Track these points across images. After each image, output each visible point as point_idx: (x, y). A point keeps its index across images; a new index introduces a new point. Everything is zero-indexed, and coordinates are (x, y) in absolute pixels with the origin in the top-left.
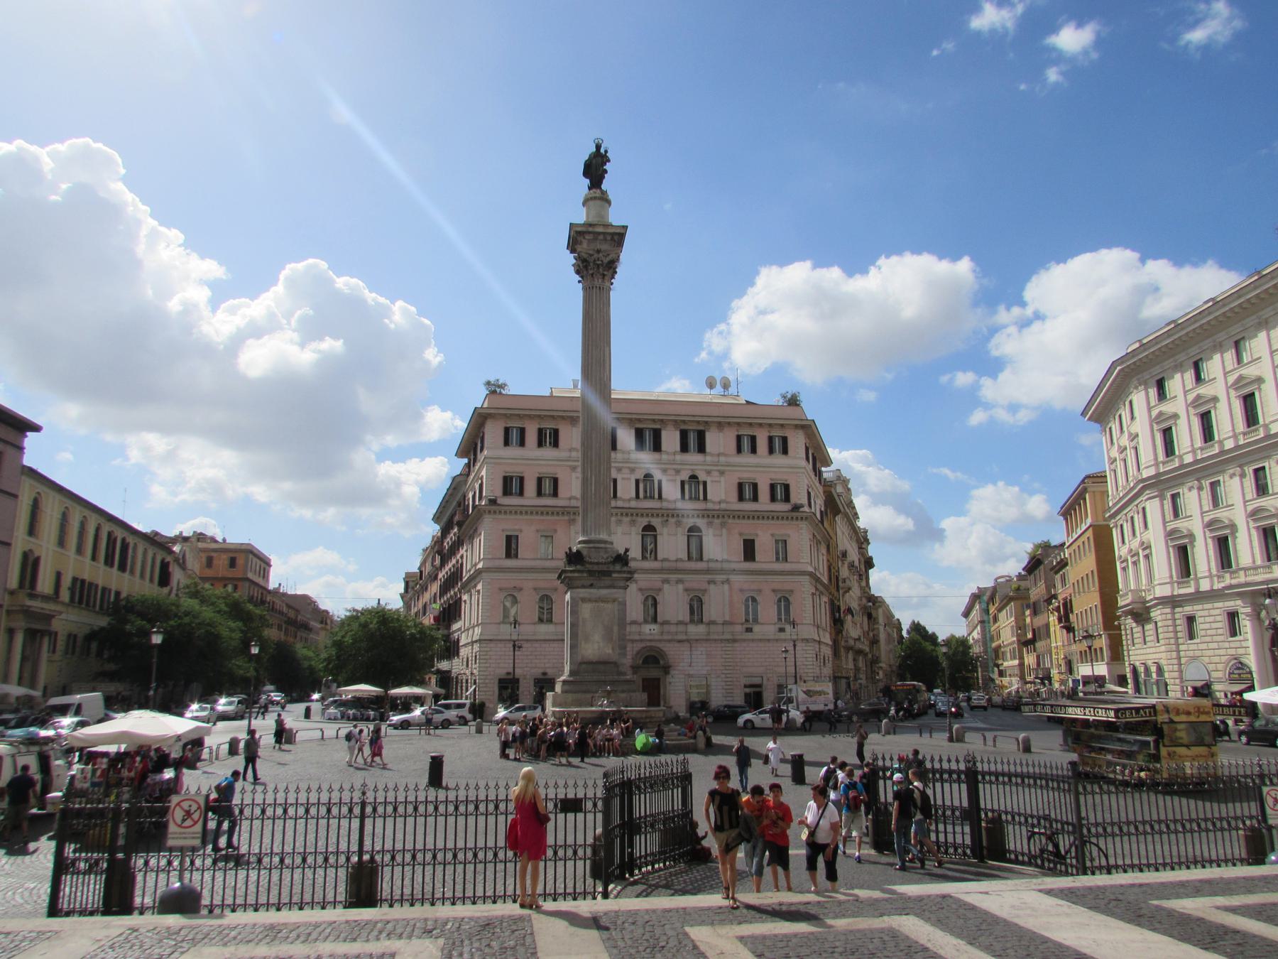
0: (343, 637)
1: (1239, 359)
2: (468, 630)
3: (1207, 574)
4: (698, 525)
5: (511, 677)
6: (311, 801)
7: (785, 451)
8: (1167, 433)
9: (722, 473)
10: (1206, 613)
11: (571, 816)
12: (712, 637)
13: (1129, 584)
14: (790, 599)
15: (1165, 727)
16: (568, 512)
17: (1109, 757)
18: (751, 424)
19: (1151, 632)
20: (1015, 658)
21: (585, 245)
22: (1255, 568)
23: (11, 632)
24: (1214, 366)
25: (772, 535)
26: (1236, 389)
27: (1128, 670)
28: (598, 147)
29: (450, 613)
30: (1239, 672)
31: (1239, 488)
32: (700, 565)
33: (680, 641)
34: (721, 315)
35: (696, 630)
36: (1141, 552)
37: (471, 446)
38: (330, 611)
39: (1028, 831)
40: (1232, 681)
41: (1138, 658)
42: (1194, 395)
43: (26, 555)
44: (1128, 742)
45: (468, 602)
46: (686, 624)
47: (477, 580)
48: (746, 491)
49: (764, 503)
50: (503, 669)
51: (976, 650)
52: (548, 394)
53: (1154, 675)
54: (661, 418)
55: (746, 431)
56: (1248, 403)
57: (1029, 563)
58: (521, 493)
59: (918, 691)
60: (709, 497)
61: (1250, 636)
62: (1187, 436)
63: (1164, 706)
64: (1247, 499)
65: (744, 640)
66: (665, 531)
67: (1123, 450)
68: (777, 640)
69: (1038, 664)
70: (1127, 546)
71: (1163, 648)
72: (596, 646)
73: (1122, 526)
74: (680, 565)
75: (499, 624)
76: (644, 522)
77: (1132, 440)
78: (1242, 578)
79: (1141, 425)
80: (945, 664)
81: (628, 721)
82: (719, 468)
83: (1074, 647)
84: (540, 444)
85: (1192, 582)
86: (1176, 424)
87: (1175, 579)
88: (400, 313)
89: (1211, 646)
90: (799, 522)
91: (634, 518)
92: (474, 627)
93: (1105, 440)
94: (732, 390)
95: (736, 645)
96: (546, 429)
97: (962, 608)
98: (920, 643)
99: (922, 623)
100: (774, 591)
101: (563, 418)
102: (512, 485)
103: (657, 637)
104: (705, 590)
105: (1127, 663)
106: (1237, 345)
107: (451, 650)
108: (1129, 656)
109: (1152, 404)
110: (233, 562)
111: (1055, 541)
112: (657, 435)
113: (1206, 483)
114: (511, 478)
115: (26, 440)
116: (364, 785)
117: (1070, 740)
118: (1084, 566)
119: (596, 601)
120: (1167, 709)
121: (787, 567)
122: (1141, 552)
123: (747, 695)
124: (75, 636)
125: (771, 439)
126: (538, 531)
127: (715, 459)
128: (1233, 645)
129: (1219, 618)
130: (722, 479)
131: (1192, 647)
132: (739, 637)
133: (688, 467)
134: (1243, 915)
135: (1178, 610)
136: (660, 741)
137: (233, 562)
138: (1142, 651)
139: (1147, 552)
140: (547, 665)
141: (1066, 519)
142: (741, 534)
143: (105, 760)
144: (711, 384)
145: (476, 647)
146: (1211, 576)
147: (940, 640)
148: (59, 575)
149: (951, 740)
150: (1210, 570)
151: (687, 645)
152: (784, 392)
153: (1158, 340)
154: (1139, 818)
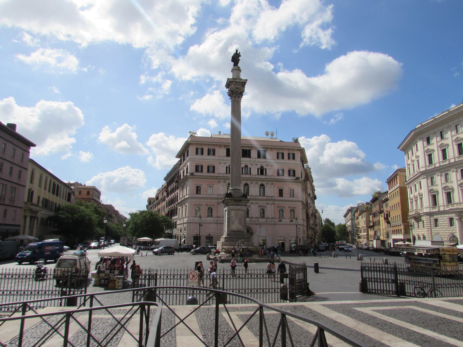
1: (457, 132)
3: (442, 205)
4: (264, 184)
7: (294, 158)
8: (430, 156)
10: (442, 218)
12: (268, 223)
13: (413, 209)
14: (295, 210)
15: (442, 256)
18: (282, 149)
19: (421, 224)
20: (365, 232)
21: (232, 85)
22: (460, 203)
23: (25, 217)
28: (237, 51)
29: (173, 212)
30: (453, 238)
31: (455, 176)
32: (264, 198)
35: (262, 220)
37: (183, 154)
40: (450, 241)
41: (416, 233)
43: (29, 190)
44: (429, 260)
46: (259, 218)
50: (196, 232)
51: (349, 229)
55: (280, 151)
57: (372, 199)
58: (202, 171)
60: (252, 173)
61: (457, 226)
62: (437, 158)
64: (458, 179)
65: (278, 224)
66: (252, 185)
67: (413, 161)
70: (413, 194)
71: (426, 230)
73: (411, 187)
74: (257, 198)
76: (260, 183)
77: (417, 158)
78: (455, 207)
83: (390, 229)
84: (209, 154)
86: (433, 153)
87: (431, 206)
89: (443, 229)
91: (257, 181)
92: (184, 218)
93: (406, 157)
95: (276, 226)
98: (329, 226)
99: (330, 219)
100: (289, 207)
101: (217, 145)
102: (198, 168)
105: (411, 235)
107: (172, 226)
109: (425, 146)
110: (88, 193)
113: (443, 174)
114: (198, 166)
115: (30, 149)
117: (407, 261)
118: (396, 200)
119: (236, 210)
120: (443, 250)
121: (294, 199)
124: (43, 219)
125: (289, 154)
126: (207, 185)
128: (451, 229)
129: (446, 220)
131: (436, 230)
132: (277, 223)
137: (88, 193)
138: (417, 231)
139: (421, 197)
141: (389, 184)
142: (278, 187)
143: (110, 261)
144: (267, 134)
145: (185, 225)
147: (336, 225)
148: (39, 197)
149: (358, 259)
150: (444, 203)
152: (293, 137)
154: (442, 283)
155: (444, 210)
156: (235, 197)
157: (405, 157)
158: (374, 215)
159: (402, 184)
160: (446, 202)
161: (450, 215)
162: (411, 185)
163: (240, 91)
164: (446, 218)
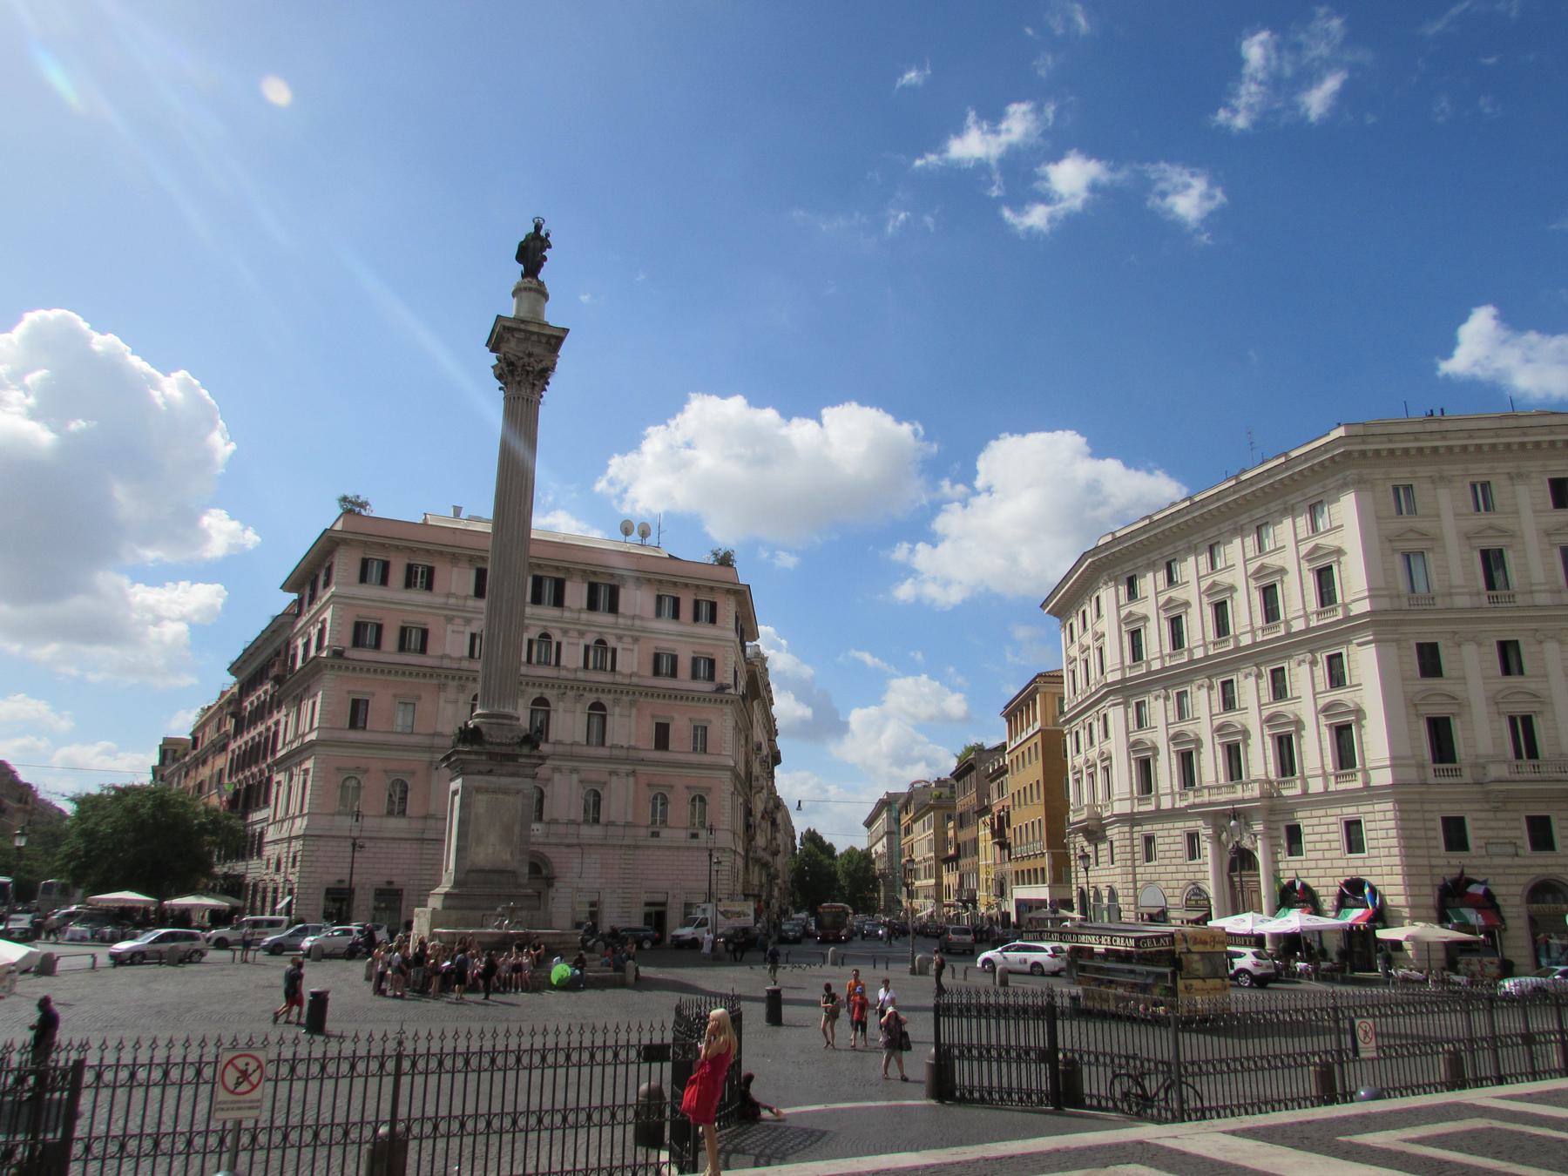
0: (97, 824)
1: (1314, 528)
2: (283, 821)
3: (1169, 791)
5: (346, 885)
6: (140, 1060)
7: (713, 619)
8: (1135, 635)
9: (636, 640)
10: (1165, 833)
11: (656, 1066)
16: (443, 676)
17: (1120, 991)
18: (675, 584)
19: (1105, 853)
20: (930, 877)
21: (513, 344)
22: (1219, 788)
24: (1188, 569)
25: (691, 720)
26: (1208, 596)
27: (1074, 894)
28: (538, 228)
29: (251, 797)
30: (1196, 898)
33: (569, 846)
34: (631, 442)
35: (590, 832)
36: (1098, 762)
38: (34, 785)
39: (1113, 1072)
40: (1188, 907)
41: (1102, 879)
42: (1209, 581)
45: (285, 785)
46: (579, 824)
47: (305, 755)
48: (664, 664)
49: (684, 681)
50: (336, 873)
51: (880, 866)
52: (420, 521)
53: (1106, 901)
54: (566, 565)
56: (1219, 611)
58: (377, 645)
59: (847, 914)
60: (618, 668)
61: (1209, 860)
62: (1156, 640)
63: (1183, 935)
65: (648, 847)
66: (617, 710)
67: (1084, 649)
68: (688, 848)
69: (961, 884)
71: (1118, 871)
72: (490, 850)
73: (1077, 733)
74: (577, 750)
75: (333, 815)
76: (591, 698)
79: (1108, 624)
80: (843, 882)
81: (539, 948)
82: (579, 627)
83: (1008, 866)
84: (409, 584)
85: (1153, 799)
86: (1186, 613)
87: (1136, 795)
88: (172, 387)
89: (1169, 869)
90: (724, 706)
92: (294, 818)
93: (1064, 637)
94: (650, 540)
96: (417, 566)
97: (865, 817)
98: (817, 856)
99: (819, 832)
100: (688, 788)
101: (441, 553)
102: (364, 633)
103: (541, 840)
104: (605, 783)
105: (1074, 887)
106: (1211, 549)
107: (249, 845)
108: (1077, 878)
111: (991, 742)
112: (559, 586)
113: (1173, 693)
114: (365, 625)
116: (402, 1032)
119: (494, 792)
121: (705, 759)
122: (1098, 762)
123: (647, 916)
125: (697, 604)
126: (395, 696)
127: (629, 622)
128: (1191, 869)
129: (1179, 839)
130: (636, 647)
132: (640, 843)
133: (593, 629)
134: (1430, 1145)
135: (1136, 829)
136: (582, 973)
139: (1106, 763)
140: (394, 872)
142: (653, 716)
144: (627, 530)
145: (297, 845)
146: (1173, 793)
147: (837, 853)
149: (913, 972)
150: (1132, 792)
151: (578, 850)
153: (1175, 515)
155: (1173, 809)
156: (492, 743)
157: (1063, 635)
158: (962, 822)
159: (1050, 721)
160: (1179, 781)
161: (1189, 824)
162: (1077, 725)
163: (540, 366)
164: (1333, 819)
